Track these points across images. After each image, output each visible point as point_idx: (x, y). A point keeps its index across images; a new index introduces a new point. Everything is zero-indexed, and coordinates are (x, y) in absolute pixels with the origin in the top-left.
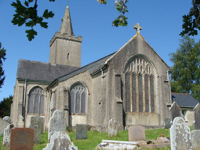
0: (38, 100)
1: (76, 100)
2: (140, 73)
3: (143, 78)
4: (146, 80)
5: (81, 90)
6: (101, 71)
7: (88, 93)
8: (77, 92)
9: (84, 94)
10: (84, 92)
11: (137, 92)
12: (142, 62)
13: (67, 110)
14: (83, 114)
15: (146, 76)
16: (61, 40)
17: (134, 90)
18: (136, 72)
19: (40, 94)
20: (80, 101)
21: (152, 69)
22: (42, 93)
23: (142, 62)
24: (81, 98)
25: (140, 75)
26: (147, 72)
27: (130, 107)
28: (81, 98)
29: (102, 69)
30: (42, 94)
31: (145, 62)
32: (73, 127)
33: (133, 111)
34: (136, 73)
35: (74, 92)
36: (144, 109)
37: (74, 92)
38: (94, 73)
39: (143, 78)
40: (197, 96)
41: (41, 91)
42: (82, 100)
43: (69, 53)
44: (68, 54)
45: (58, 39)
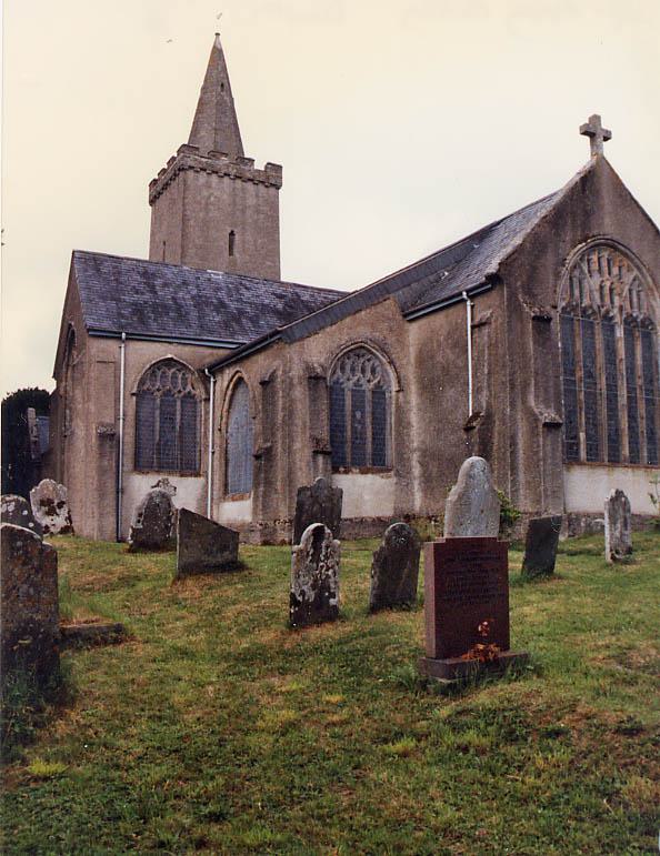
0: (174, 415)
1: (354, 416)
2: (608, 312)
3: (620, 333)
4: (629, 333)
5: (369, 375)
6: (464, 301)
7: (394, 387)
8: (355, 385)
9: (379, 392)
10: (379, 382)
11: (603, 383)
12: (615, 271)
13: (324, 453)
14: (382, 471)
15: (630, 322)
16: (203, 177)
17: (589, 377)
18: (595, 307)
19: (180, 392)
20: (368, 420)
21: (647, 296)
22: (189, 388)
23: (615, 271)
24: (368, 409)
25: (607, 318)
26: (632, 307)
27: (578, 444)
28: (368, 409)
29: (468, 291)
30: (189, 393)
31: (624, 270)
32: (346, 520)
33: (588, 460)
34: (594, 313)
35: (342, 383)
36: (626, 451)
37: (342, 383)
38: (104, 331)
39: (620, 333)
40: (566, 658)
41: (185, 379)
42: (373, 413)
43: (236, 230)
44: (232, 234)
45: (191, 174)
